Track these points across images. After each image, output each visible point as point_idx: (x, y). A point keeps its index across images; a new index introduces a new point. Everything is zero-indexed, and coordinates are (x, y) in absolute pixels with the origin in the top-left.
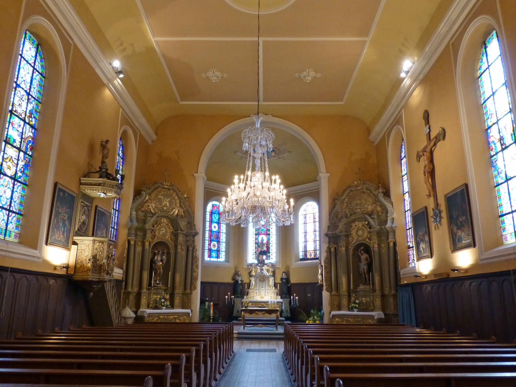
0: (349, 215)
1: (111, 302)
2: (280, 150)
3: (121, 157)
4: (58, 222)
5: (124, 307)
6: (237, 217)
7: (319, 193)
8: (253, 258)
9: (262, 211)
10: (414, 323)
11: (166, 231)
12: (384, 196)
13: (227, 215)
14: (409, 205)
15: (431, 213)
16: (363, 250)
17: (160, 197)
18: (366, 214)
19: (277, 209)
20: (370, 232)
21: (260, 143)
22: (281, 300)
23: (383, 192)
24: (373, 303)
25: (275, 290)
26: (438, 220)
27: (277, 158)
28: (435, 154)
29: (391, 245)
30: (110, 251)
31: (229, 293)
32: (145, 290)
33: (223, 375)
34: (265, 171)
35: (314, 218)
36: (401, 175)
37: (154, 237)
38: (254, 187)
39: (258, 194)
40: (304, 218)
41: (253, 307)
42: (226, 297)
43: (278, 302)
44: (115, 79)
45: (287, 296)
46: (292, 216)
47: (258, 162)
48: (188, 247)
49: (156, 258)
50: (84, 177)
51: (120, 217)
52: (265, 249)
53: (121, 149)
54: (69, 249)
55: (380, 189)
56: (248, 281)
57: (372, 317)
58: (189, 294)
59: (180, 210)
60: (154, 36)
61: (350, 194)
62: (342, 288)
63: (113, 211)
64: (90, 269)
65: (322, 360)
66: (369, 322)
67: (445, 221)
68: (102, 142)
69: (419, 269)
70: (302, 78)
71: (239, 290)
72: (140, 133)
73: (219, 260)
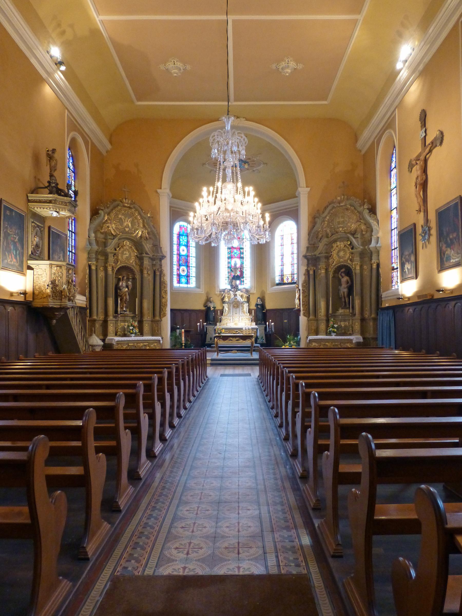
0: (330, 235)
1: (76, 329)
2: (254, 161)
3: (72, 171)
4: (8, 243)
5: (91, 335)
6: (207, 234)
7: (298, 211)
8: (226, 284)
9: (234, 228)
10: (393, 345)
11: (130, 254)
12: (370, 212)
13: (196, 232)
14: (396, 222)
15: (419, 230)
16: (344, 272)
17: (120, 216)
18: (348, 233)
19: (251, 225)
20: (352, 253)
21: (231, 148)
22: (256, 327)
23: (368, 209)
24: (352, 327)
25: (249, 317)
26: (427, 237)
27: (251, 171)
28: (430, 163)
29: (375, 266)
30: (69, 276)
31: (201, 320)
32: (111, 318)
33: (198, 398)
34: (237, 181)
35: (292, 239)
36: (389, 188)
37: (116, 261)
38: (225, 200)
39: (230, 207)
40: (280, 240)
41: (226, 334)
42: (199, 324)
43: (252, 329)
44: (55, 72)
45: (262, 322)
46: (267, 233)
47: (229, 172)
48: (155, 272)
49: (121, 284)
50: (32, 193)
51: (77, 238)
52: (238, 273)
53: (71, 161)
54: (24, 275)
55: (365, 205)
56: (221, 308)
57: (350, 341)
58: (158, 321)
59: (144, 231)
60: (98, 14)
61: (332, 212)
62: (321, 312)
63: (69, 233)
64: (50, 296)
65: (297, 378)
66: (348, 346)
67: (434, 239)
68: (48, 151)
69: (402, 291)
70: (280, 70)
71: (211, 317)
72: (91, 141)
73: (189, 286)
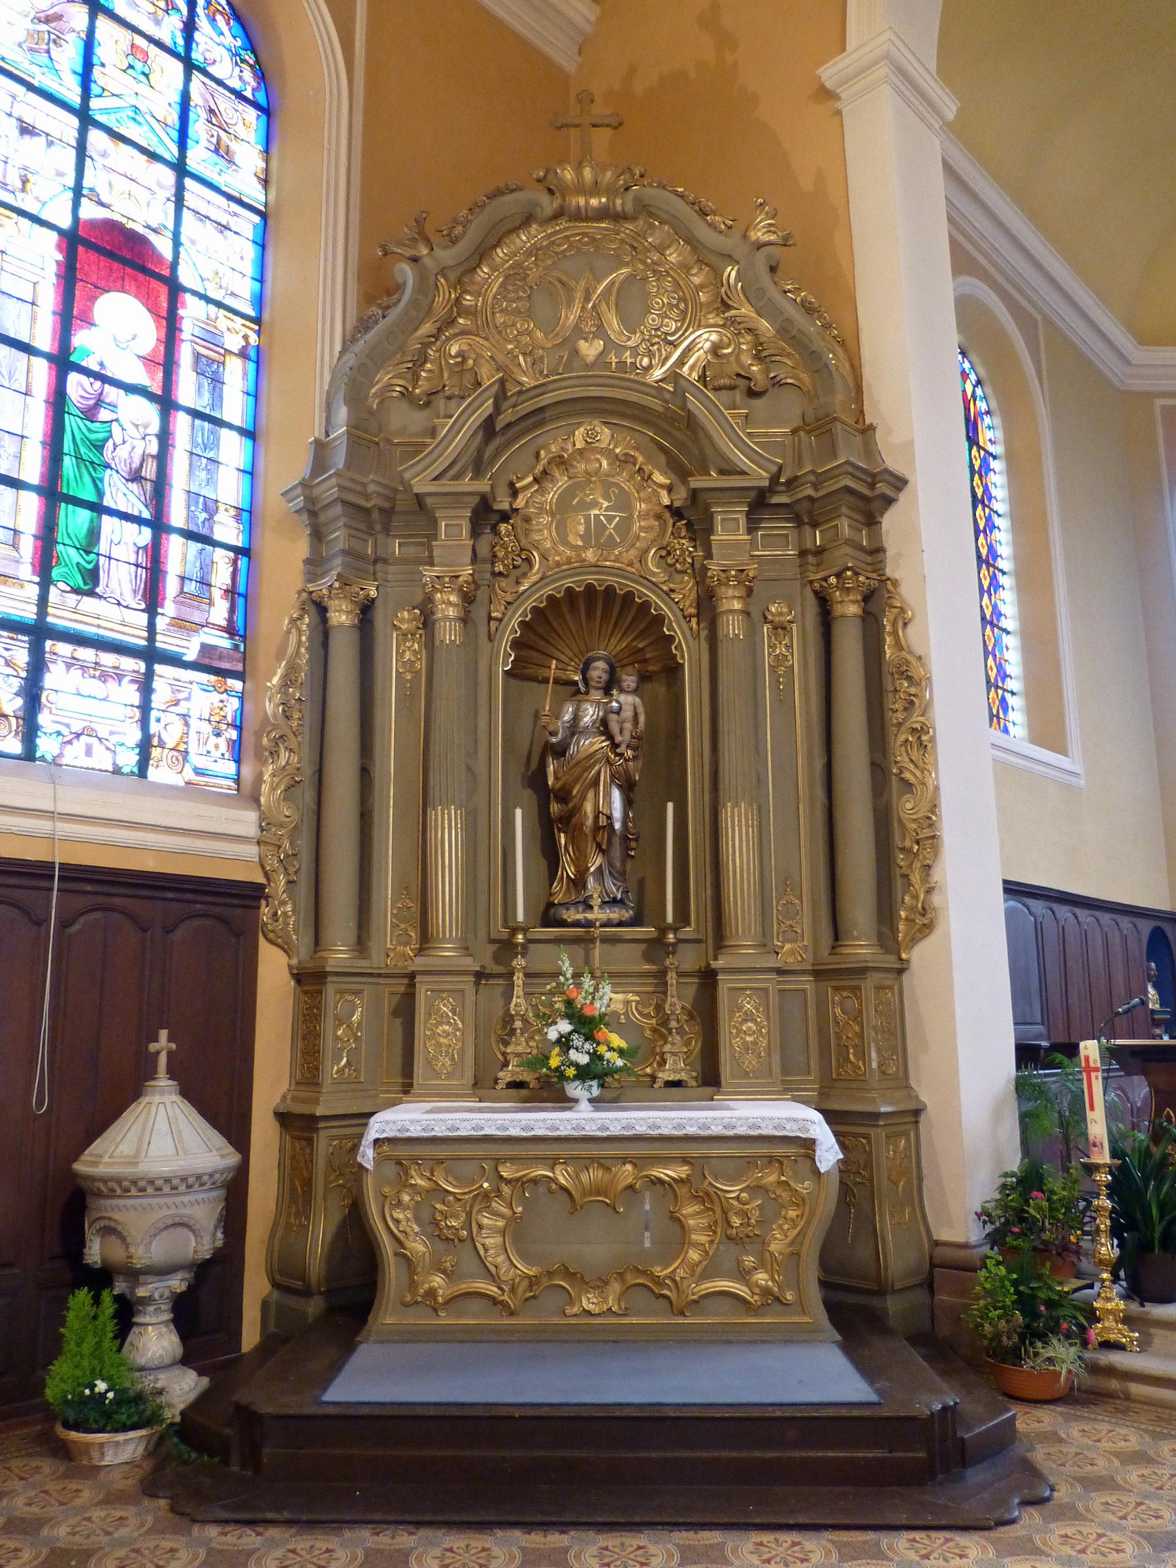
48: (824, 602)
